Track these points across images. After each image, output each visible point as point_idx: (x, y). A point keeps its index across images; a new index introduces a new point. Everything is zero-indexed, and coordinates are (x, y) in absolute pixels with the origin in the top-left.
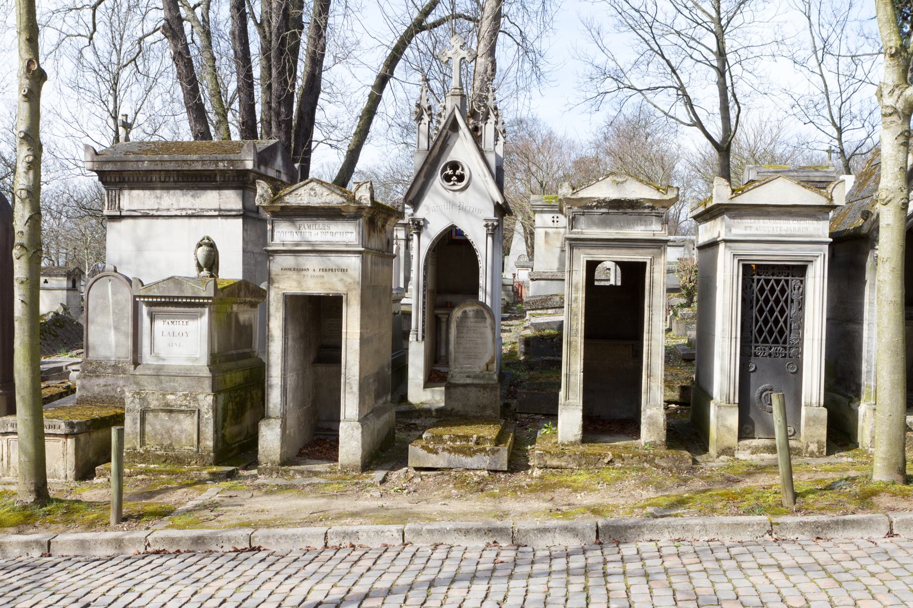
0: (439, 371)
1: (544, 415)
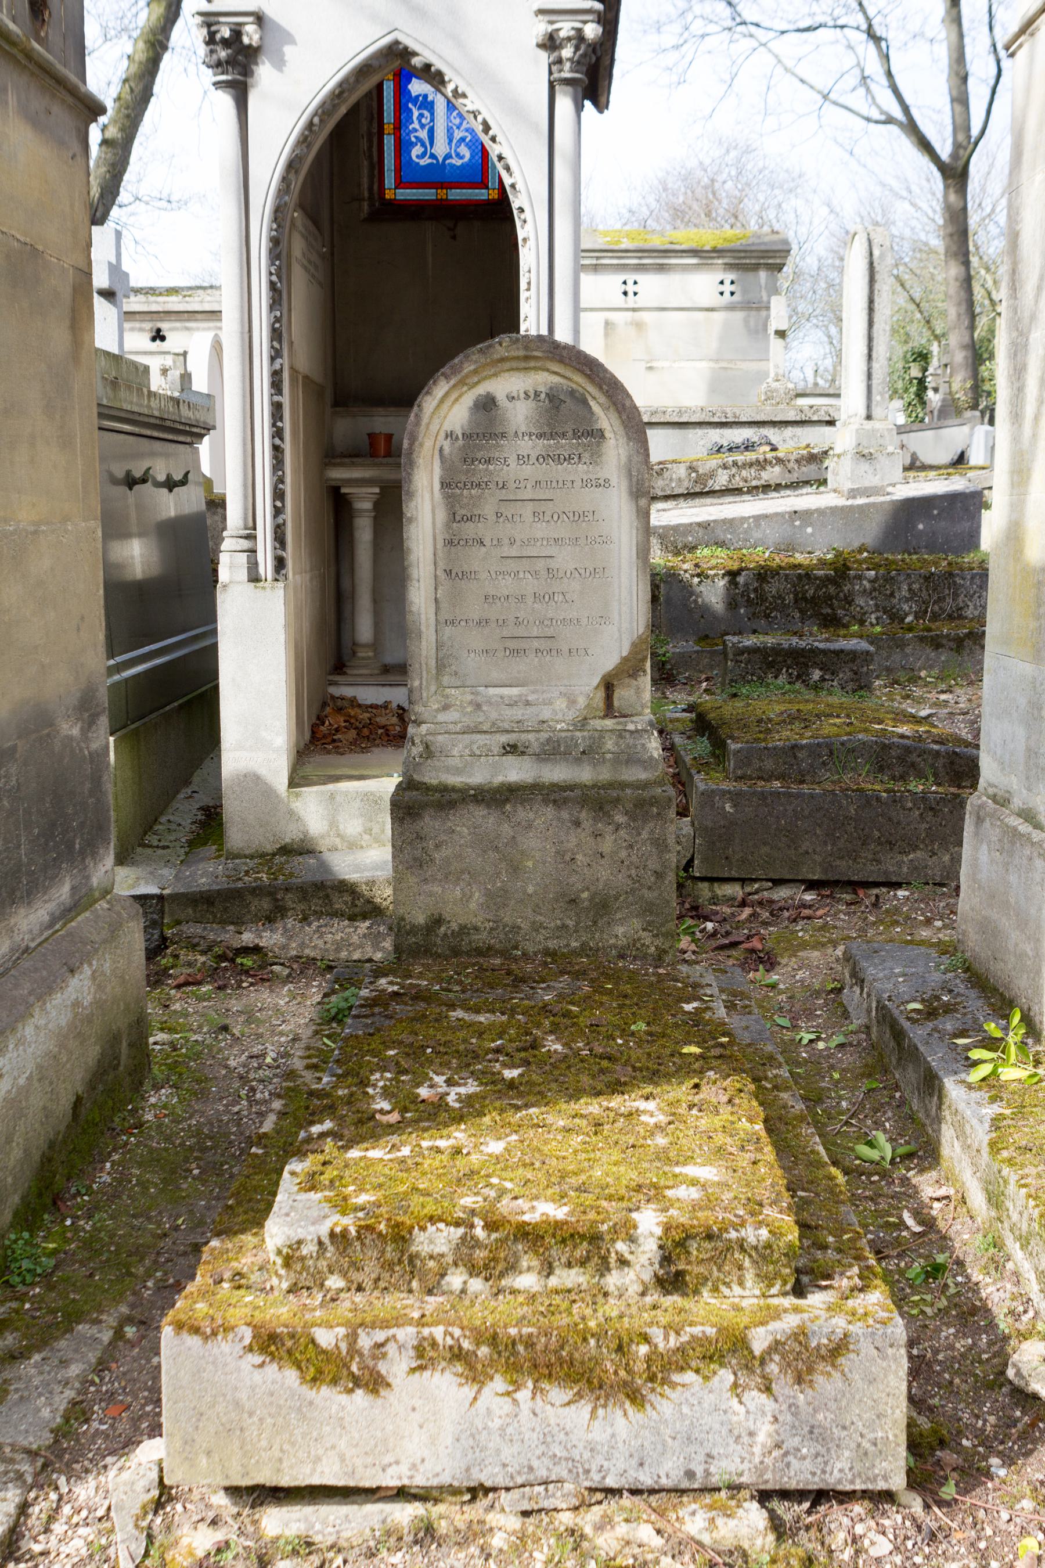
0: (353, 702)
1: (811, 885)
